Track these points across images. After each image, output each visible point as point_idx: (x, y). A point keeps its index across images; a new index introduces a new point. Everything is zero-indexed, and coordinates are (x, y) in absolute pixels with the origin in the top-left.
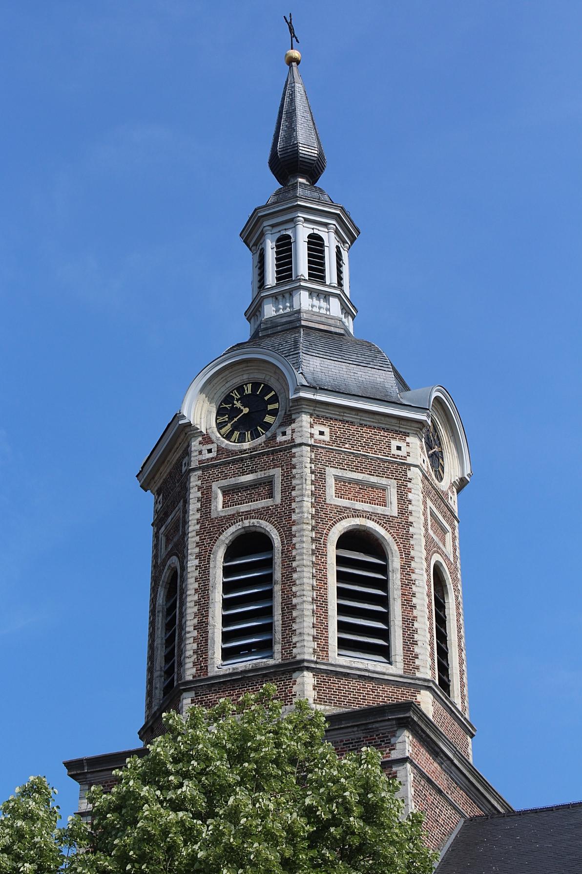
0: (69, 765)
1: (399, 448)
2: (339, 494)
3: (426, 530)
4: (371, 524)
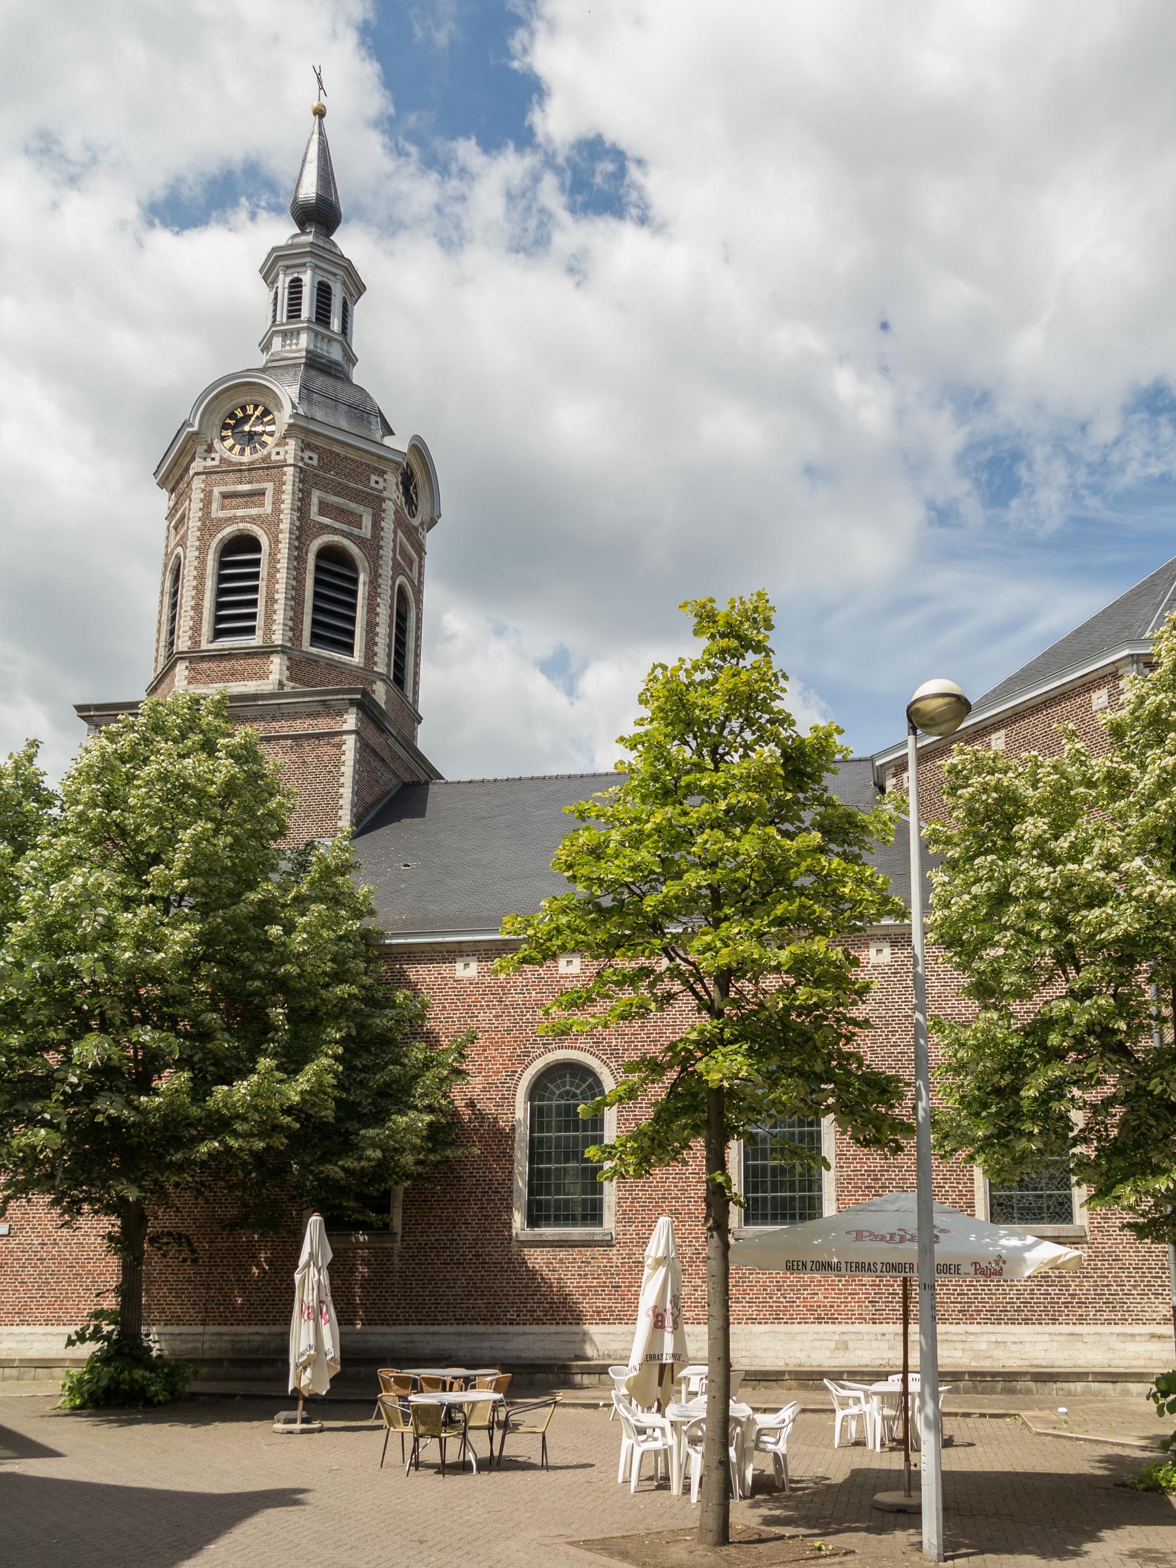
0: (79, 708)
1: (377, 482)
2: (321, 512)
3: (395, 554)
4: (347, 543)
